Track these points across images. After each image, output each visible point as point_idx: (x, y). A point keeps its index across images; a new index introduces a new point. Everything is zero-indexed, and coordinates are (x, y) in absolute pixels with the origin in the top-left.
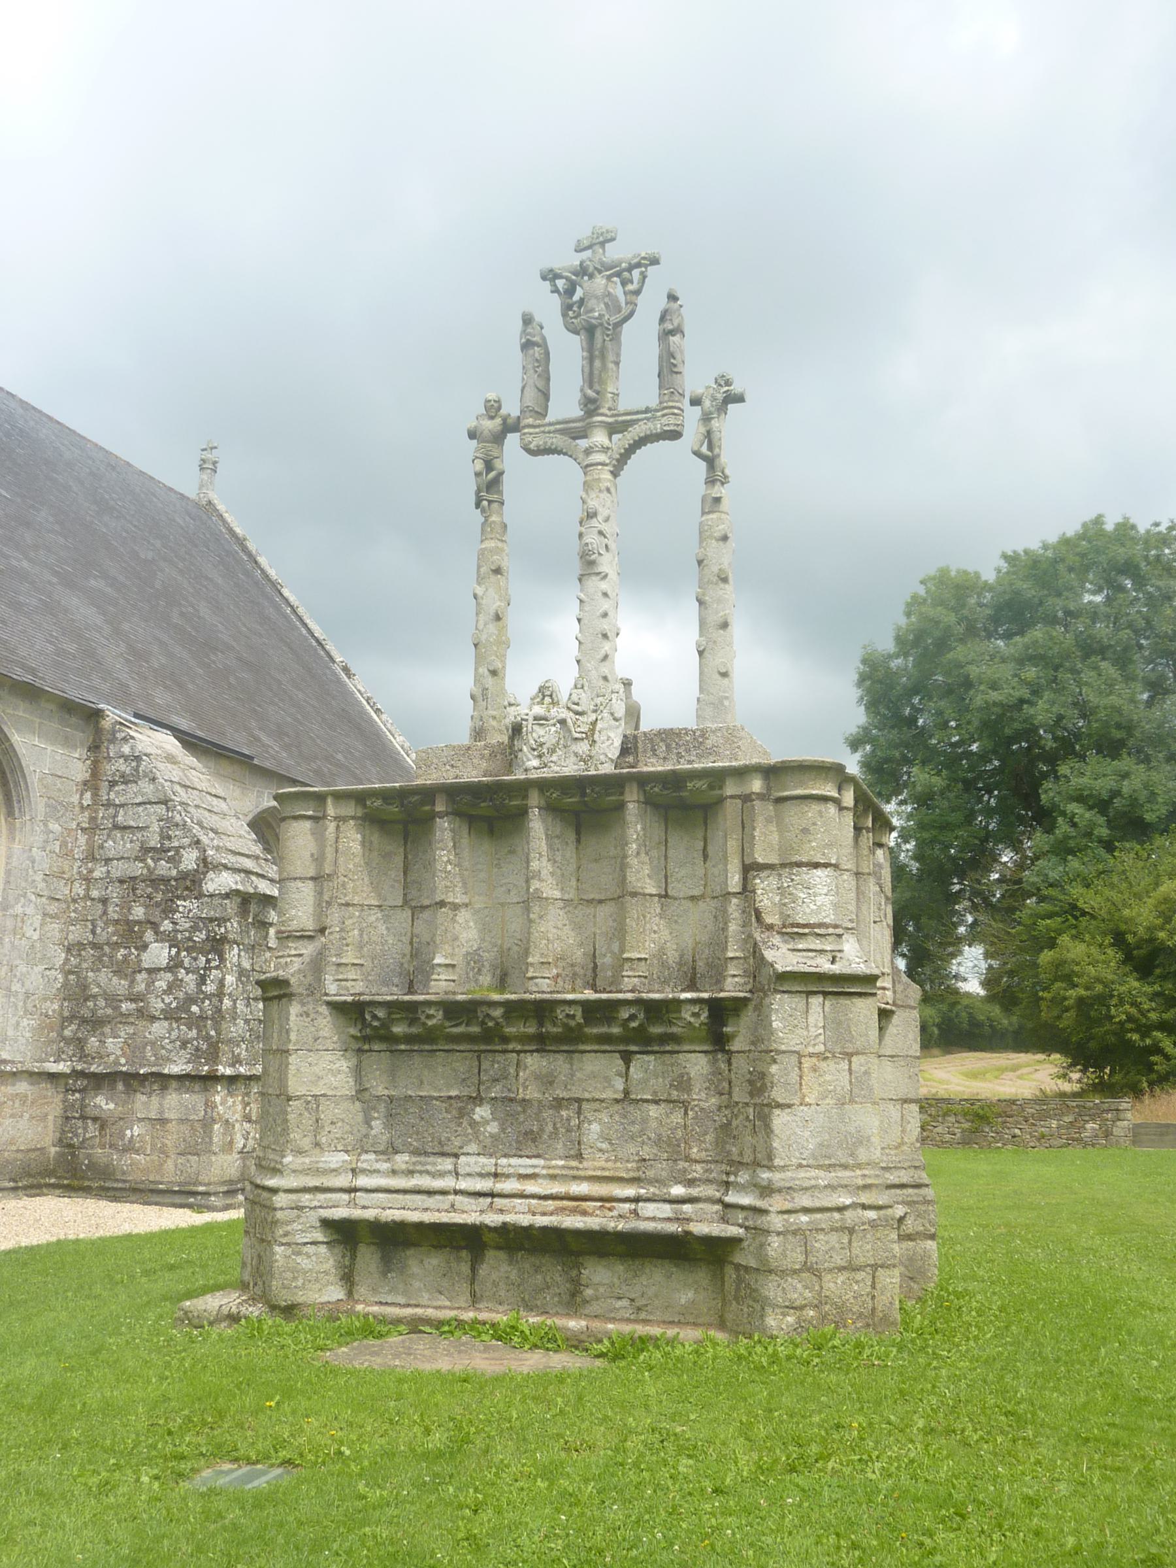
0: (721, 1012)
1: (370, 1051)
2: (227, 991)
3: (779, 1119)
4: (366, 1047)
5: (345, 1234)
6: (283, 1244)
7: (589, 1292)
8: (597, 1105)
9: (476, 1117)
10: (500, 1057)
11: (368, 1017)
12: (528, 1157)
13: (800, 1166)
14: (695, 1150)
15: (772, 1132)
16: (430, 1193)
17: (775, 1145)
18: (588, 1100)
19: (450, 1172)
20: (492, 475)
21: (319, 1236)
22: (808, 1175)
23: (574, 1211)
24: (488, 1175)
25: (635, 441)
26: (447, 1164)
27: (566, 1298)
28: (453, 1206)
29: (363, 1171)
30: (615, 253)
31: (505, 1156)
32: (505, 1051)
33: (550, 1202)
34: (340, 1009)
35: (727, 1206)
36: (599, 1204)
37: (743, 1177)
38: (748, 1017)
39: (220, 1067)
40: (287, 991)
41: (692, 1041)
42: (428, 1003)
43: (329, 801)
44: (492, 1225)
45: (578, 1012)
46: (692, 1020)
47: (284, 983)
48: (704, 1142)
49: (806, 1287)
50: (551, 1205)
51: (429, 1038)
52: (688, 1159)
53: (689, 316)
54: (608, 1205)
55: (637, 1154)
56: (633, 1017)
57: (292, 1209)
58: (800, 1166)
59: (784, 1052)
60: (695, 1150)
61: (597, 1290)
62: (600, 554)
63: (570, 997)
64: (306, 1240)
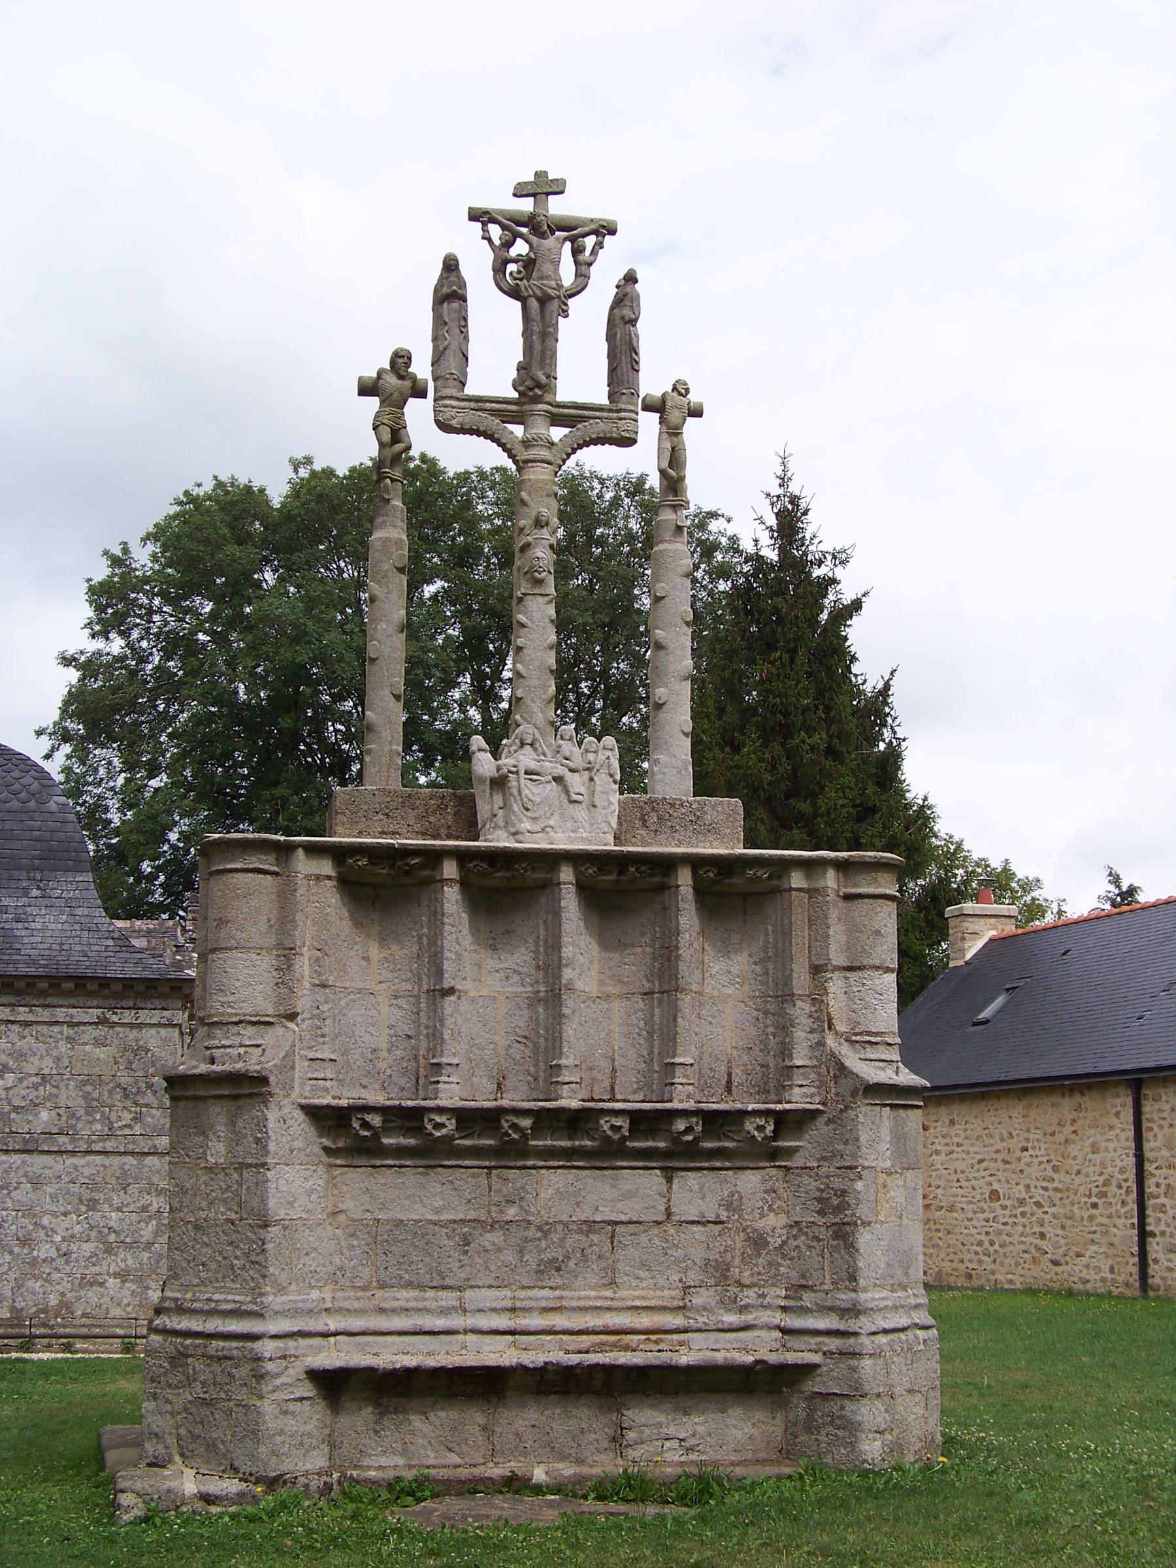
0: (790, 1122)
3: (863, 1238)
5: (333, 1385)
7: (631, 1435)
12: (551, 1288)
13: (875, 1285)
14: (746, 1274)
15: (857, 1250)
18: (622, 1223)
20: (399, 447)
23: (614, 1346)
24: (504, 1309)
26: (449, 1298)
29: (340, 1310)
30: (557, 207)
33: (584, 1337)
36: (644, 1337)
37: (808, 1299)
38: (821, 1129)
42: (441, 1110)
44: (531, 1366)
46: (609, 1133)
47: (263, 1080)
48: (756, 1265)
50: (585, 1341)
52: (739, 1283)
55: (681, 1281)
56: (689, 1130)
60: (746, 1274)
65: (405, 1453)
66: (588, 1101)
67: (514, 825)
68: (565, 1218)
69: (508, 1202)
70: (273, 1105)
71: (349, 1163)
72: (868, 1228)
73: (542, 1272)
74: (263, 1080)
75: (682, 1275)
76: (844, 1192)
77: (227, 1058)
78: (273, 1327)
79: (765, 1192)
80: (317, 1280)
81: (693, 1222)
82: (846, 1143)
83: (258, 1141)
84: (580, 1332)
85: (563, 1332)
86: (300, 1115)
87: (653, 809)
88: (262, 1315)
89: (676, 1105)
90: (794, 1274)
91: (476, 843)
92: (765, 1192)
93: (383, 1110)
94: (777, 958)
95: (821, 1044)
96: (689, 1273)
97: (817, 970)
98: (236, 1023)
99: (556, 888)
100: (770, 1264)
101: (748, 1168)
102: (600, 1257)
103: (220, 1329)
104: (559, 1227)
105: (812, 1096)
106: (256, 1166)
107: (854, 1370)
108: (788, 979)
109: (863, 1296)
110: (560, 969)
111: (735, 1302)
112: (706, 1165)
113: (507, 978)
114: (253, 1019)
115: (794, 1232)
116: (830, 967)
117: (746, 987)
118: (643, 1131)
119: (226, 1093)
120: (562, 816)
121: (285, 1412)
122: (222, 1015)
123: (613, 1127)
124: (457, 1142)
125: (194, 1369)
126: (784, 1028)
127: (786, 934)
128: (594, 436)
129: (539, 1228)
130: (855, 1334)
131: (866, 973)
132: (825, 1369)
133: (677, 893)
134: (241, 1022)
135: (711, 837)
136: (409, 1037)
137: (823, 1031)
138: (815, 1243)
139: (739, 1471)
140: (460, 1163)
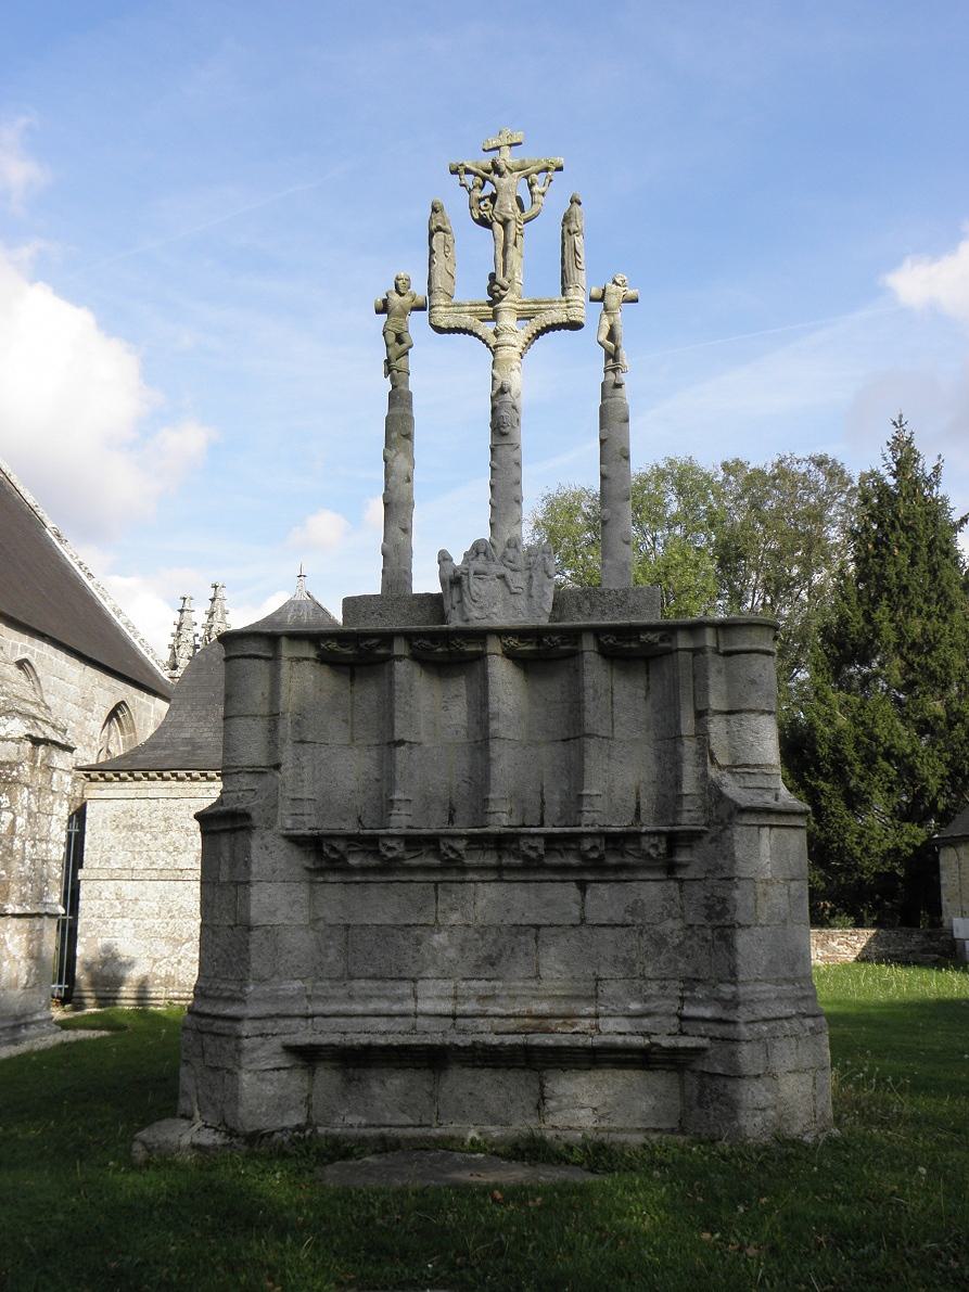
0: (674, 840)
1: (325, 882)
2: (18, 832)
3: (742, 940)
4: (321, 879)
5: (306, 1056)
6: (250, 1071)
7: (552, 1104)
8: (553, 931)
9: (435, 944)
10: (455, 887)
11: (326, 849)
12: (487, 979)
13: (756, 980)
14: (649, 969)
15: (736, 950)
17: (739, 962)
18: (545, 926)
19: (409, 996)
21: (281, 1061)
22: (764, 988)
25: (548, 326)
26: (405, 988)
27: (531, 1110)
28: (414, 1028)
29: (318, 997)
31: (465, 979)
33: (512, 1020)
34: (295, 840)
35: (682, 1018)
36: (561, 1021)
37: (700, 992)
38: (705, 847)
39: (10, 906)
40: (248, 824)
41: (649, 868)
43: (284, 641)
44: (461, 1044)
45: (540, 844)
47: (246, 816)
49: (767, 1090)
51: (388, 867)
52: (643, 977)
54: (569, 1022)
55: (594, 974)
56: (594, 848)
57: (257, 1036)
58: (756, 980)
59: (743, 879)
60: (649, 969)
61: (561, 1101)
62: (513, 427)
63: (533, 830)
64: (268, 1067)
66: (520, 826)
68: (497, 922)
69: (451, 909)
70: (255, 836)
71: (599, 877)
72: (747, 931)
75: (596, 970)
76: (724, 900)
78: (252, 1010)
79: (664, 900)
80: (300, 973)
81: (604, 925)
82: (725, 858)
84: (508, 1016)
85: (495, 1016)
86: (283, 843)
87: (586, 598)
88: (244, 1001)
89: (390, 831)
90: (690, 969)
92: (664, 900)
93: (349, 838)
94: (668, 709)
95: (705, 775)
96: (602, 967)
97: (701, 715)
98: (237, 773)
100: (670, 961)
101: (648, 880)
102: (526, 954)
104: (494, 930)
105: (698, 820)
107: (733, 1054)
108: (678, 724)
109: (742, 990)
110: (488, 722)
111: (640, 992)
112: (612, 877)
113: (457, 732)
115: (689, 933)
116: (710, 712)
118: (559, 851)
121: (263, 1080)
123: (531, 848)
124: (407, 862)
126: (677, 764)
127: (675, 686)
130: (735, 1023)
131: (743, 716)
133: (583, 657)
137: (706, 764)
138: (704, 943)
139: (621, 1137)
140: (412, 878)
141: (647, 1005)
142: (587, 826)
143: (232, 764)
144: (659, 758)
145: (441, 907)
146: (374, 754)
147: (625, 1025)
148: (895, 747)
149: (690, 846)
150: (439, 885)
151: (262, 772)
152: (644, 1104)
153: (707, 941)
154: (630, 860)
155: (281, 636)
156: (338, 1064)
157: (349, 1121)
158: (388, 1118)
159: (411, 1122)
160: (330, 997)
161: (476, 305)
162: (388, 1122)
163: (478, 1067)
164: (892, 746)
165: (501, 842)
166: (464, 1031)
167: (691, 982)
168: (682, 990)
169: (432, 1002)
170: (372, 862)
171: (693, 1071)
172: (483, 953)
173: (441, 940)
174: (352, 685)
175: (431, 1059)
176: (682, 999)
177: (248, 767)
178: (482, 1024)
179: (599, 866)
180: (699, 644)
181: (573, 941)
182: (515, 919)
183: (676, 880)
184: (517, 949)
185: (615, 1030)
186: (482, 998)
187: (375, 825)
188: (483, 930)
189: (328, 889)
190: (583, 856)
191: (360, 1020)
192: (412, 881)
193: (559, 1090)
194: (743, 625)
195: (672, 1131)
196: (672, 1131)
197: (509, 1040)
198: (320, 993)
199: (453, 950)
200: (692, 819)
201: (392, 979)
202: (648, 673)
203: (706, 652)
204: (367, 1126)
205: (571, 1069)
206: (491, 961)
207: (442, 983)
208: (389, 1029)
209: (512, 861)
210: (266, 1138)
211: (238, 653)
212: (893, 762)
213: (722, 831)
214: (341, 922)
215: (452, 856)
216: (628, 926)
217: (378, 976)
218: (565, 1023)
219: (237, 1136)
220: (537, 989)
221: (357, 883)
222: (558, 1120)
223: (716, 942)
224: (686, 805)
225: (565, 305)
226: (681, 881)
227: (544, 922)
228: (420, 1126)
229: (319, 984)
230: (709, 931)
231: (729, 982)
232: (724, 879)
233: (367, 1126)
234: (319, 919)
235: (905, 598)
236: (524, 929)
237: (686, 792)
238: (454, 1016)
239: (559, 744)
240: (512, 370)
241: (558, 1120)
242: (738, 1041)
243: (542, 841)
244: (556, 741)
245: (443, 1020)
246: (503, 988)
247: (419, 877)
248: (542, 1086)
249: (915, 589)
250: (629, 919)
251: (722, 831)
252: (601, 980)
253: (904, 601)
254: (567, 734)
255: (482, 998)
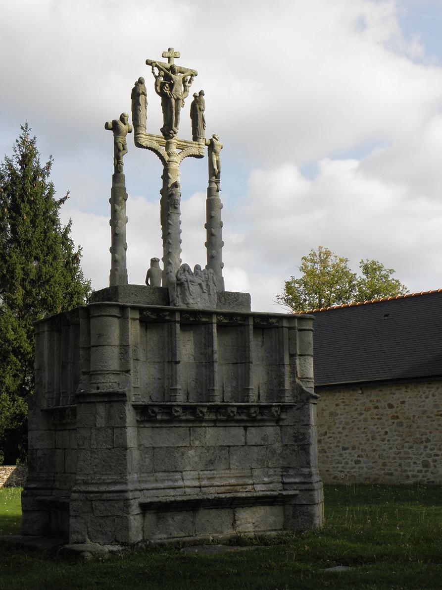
4: (142, 426)
5: (145, 508)
7: (238, 522)
10: (198, 429)
12: (210, 470)
15: (310, 454)
16: (157, 489)
26: (178, 476)
27: (230, 526)
28: (185, 493)
31: (202, 471)
32: (200, 427)
35: (283, 483)
37: (292, 472)
42: (178, 406)
45: (235, 410)
52: (268, 467)
53: (208, 101)
54: (244, 487)
60: (270, 463)
65: (166, 533)
67: (186, 301)
68: (214, 445)
71: (252, 425)
73: (207, 464)
74: (124, 395)
76: (304, 434)
77: (105, 387)
79: (275, 434)
81: (254, 445)
82: (305, 416)
83: (121, 418)
84: (221, 486)
89: (250, 404)
90: (285, 463)
91: (169, 307)
95: (294, 382)
97: (292, 356)
98: (108, 374)
99: (210, 325)
102: (225, 459)
103: (107, 489)
104: (212, 448)
105: (291, 400)
106: (120, 427)
107: (312, 495)
112: (257, 425)
114: (114, 372)
115: (285, 448)
117: (264, 361)
119: (106, 400)
120: (201, 298)
122: (101, 371)
125: (95, 505)
128: (191, 154)
129: (206, 449)
131: (306, 357)
132: (300, 496)
134: (110, 373)
135: (241, 306)
136: (160, 379)
137: (295, 377)
139: (268, 533)
140: (181, 425)
141: (270, 479)
142: (252, 402)
143: (105, 369)
144: (268, 373)
145: (192, 438)
146: (156, 366)
147: (264, 487)
148: (22, 348)
149: (286, 412)
150: (191, 428)
151: (118, 374)
152: (271, 519)
153: (295, 451)
154: (265, 417)
155: (128, 307)
156: (155, 511)
157: (159, 537)
158: (175, 534)
159: (184, 535)
160: (148, 481)
161: (159, 137)
162: (175, 536)
163: (210, 508)
164: (20, 347)
165: (216, 409)
166: (205, 493)
167: (286, 469)
168: (282, 472)
169: (189, 482)
170: (165, 417)
171: (290, 504)
172: (208, 459)
173: (192, 453)
174: (146, 332)
175: (192, 506)
176: (282, 476)
177: (113, 371)
178: (212, 490)
179: (253, 420)
180: (292, 326)
181: (242, 453)
182: (220, 443)
183: (279, 426)
184: (221, 457)
185: (260, 490)
186: (209, 479)
187: (158, 400)
188: (208, 448)
189: (145, 430)
190: (249, 415)
191: (163, 491)
192: (180, 427)
193: (241, 517)
194: (308, 319)
195: (281, 530)
196: (281, 530)
197: (223, 496)
198: (143, 479)
199: (196, 458)
200: (289, 400)
201: (172, 472)
202: (263, 335)
203: (295, 329)
204: (167, 538)
205: (245, 507)
206: (211, 462)
207: (193, 472)
208: (175, 494)
209: (222, 417)
210: (136, 546)
211: (108, 314)
212: (20, 357)
213: (303, 406)
214: (151, 446)
215: (201, 415)
216: (262, 445)
217: (166, 471)
218: (242, 488)
219: (128, 546)
220: (230, 474)
221: (158, 427)
222: (240, 529)
223: (300, 452)
224: (287, 394)
225: (197, 146)
226: (281, 426)
227: (232, 444)
228: (188, 536)
229: (142, 475)
230: (296, 447)
231: (306, 467)
232: (304, 425)
233: (167, 538)
234: (141, 445)
235: (28, 248)
236: (223, 448)
237: (287, 389)
238: (200, 487)
239: (231, 365)
240: (178, 175)
241: (240, 529)
242: (314, 490)
243: (236, 409)
244: (229, 364)
245: (195, 489)
246: (217, 474)
247: (183, 425)
248: (235, 515)
249: (34, 243)
250: (263, 443)
251: (304, 405)
252: (252, 469)
253: (28, 250)
254: (235, 361)
255: (209, 479)
